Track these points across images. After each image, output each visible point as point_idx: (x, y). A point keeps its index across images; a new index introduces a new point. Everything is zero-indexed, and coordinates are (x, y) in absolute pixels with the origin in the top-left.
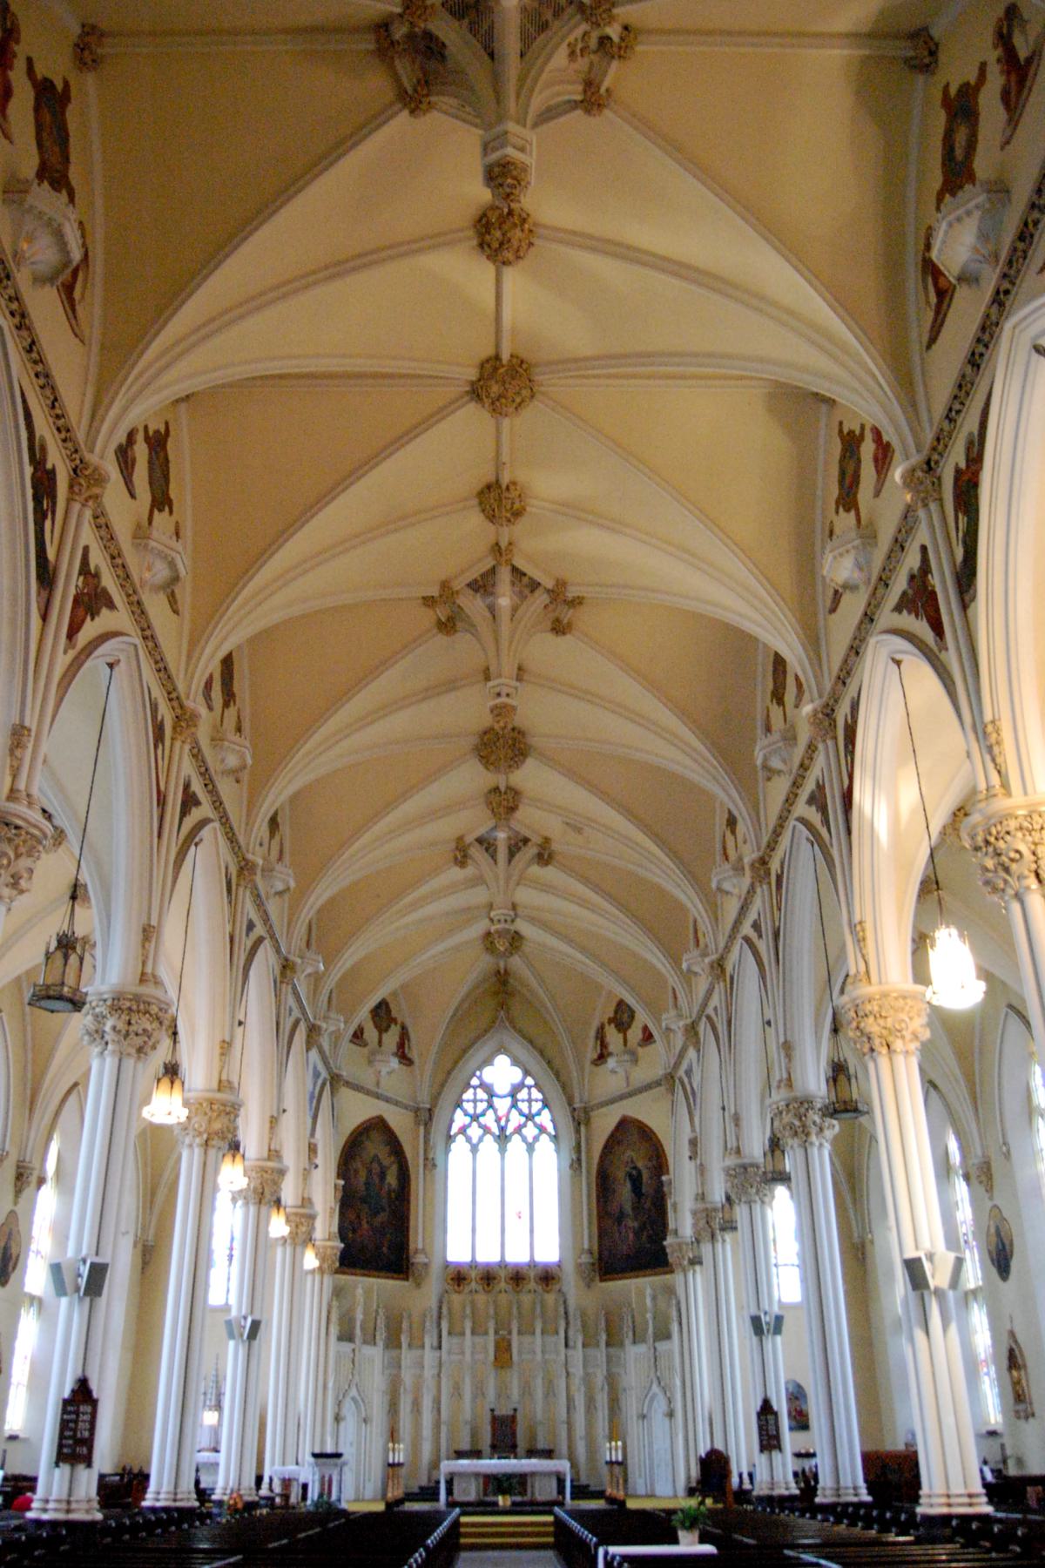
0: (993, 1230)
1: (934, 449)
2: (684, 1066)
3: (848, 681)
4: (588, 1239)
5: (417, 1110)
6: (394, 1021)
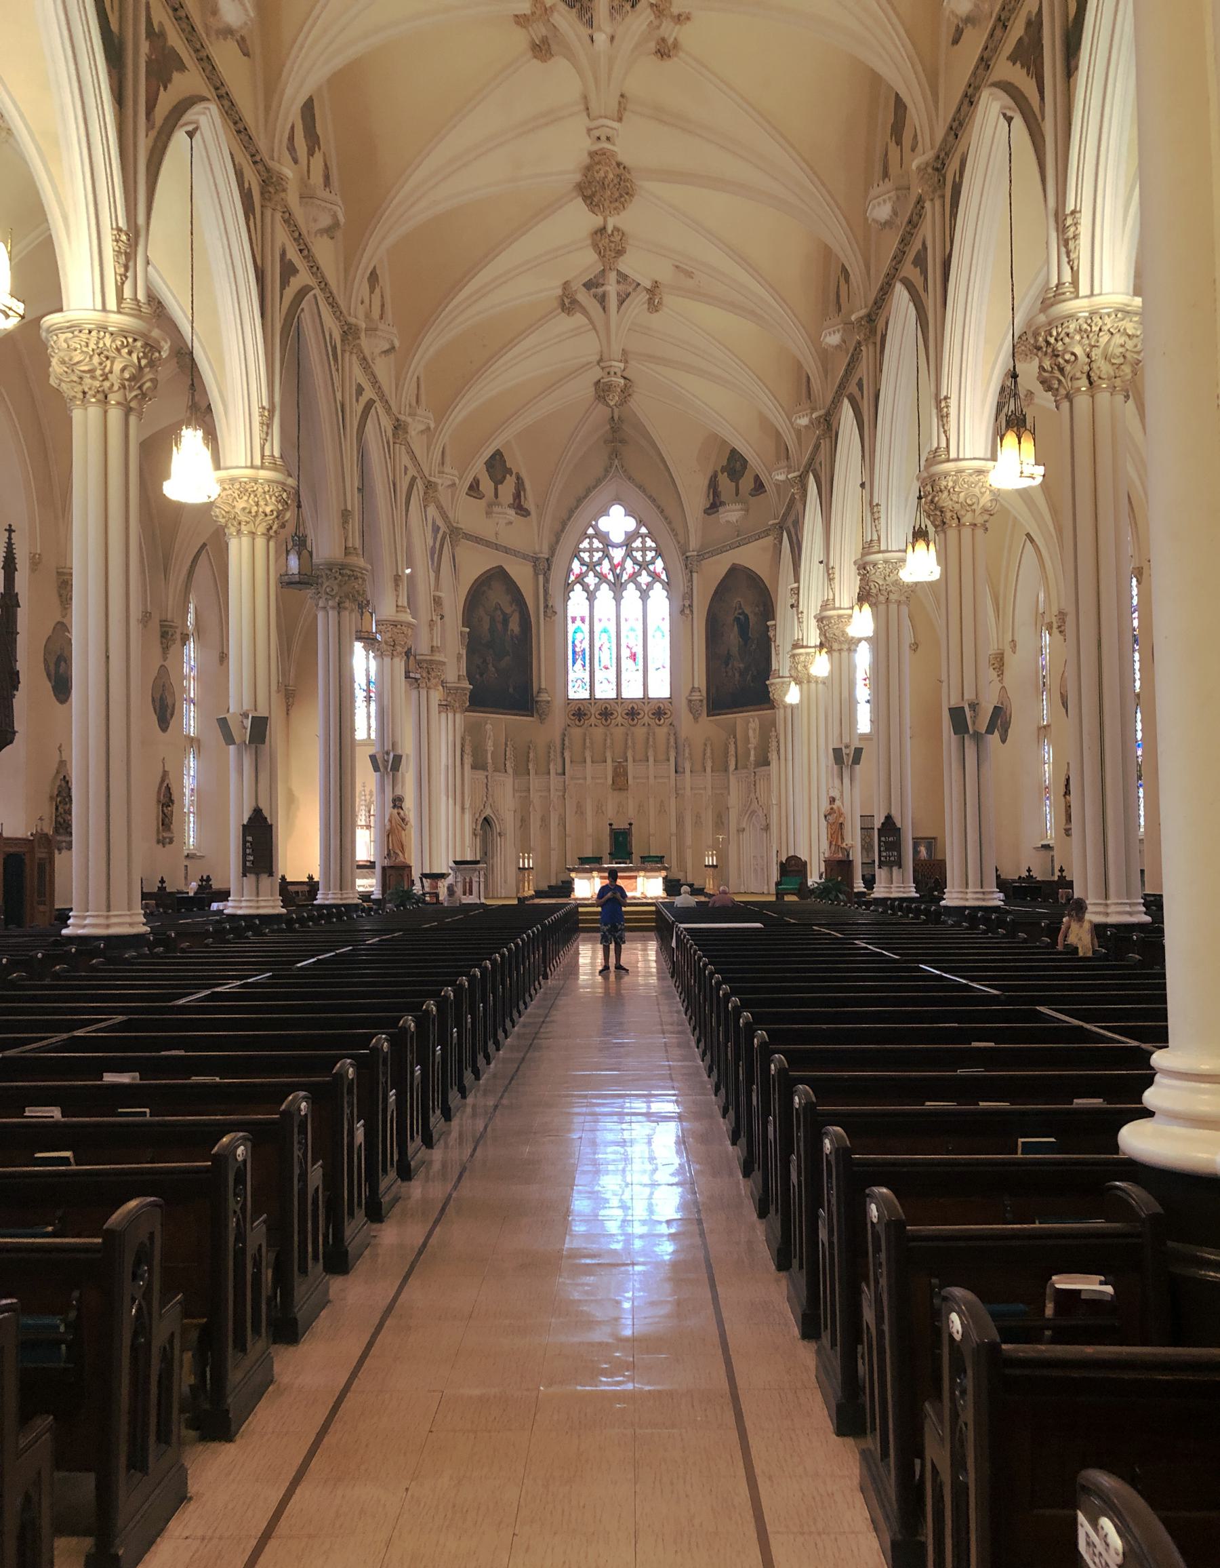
4: (700, 681)
5: (535, 560)
6: (510, 472)
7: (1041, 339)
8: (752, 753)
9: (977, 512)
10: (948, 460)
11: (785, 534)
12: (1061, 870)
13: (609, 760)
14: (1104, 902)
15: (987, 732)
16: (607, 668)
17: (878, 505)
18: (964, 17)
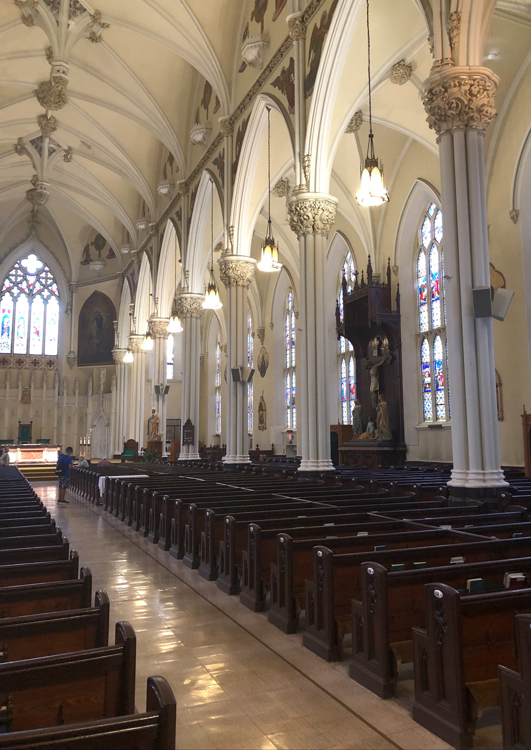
0: (261, 356)
1: (306, 11)
2: (130, 271)
3: (243, 111)
4: (75, 348)
7: (293, 207)
8: (102, 386)
9: (245, 280)
10: (232, 255)
11: (126, 279)
12: (257, 446)
13: (20, 387)
14: (316, 461)
15: (248, 381)
16: (22, 338)
17: (188, 271)
18: (249, 61)
